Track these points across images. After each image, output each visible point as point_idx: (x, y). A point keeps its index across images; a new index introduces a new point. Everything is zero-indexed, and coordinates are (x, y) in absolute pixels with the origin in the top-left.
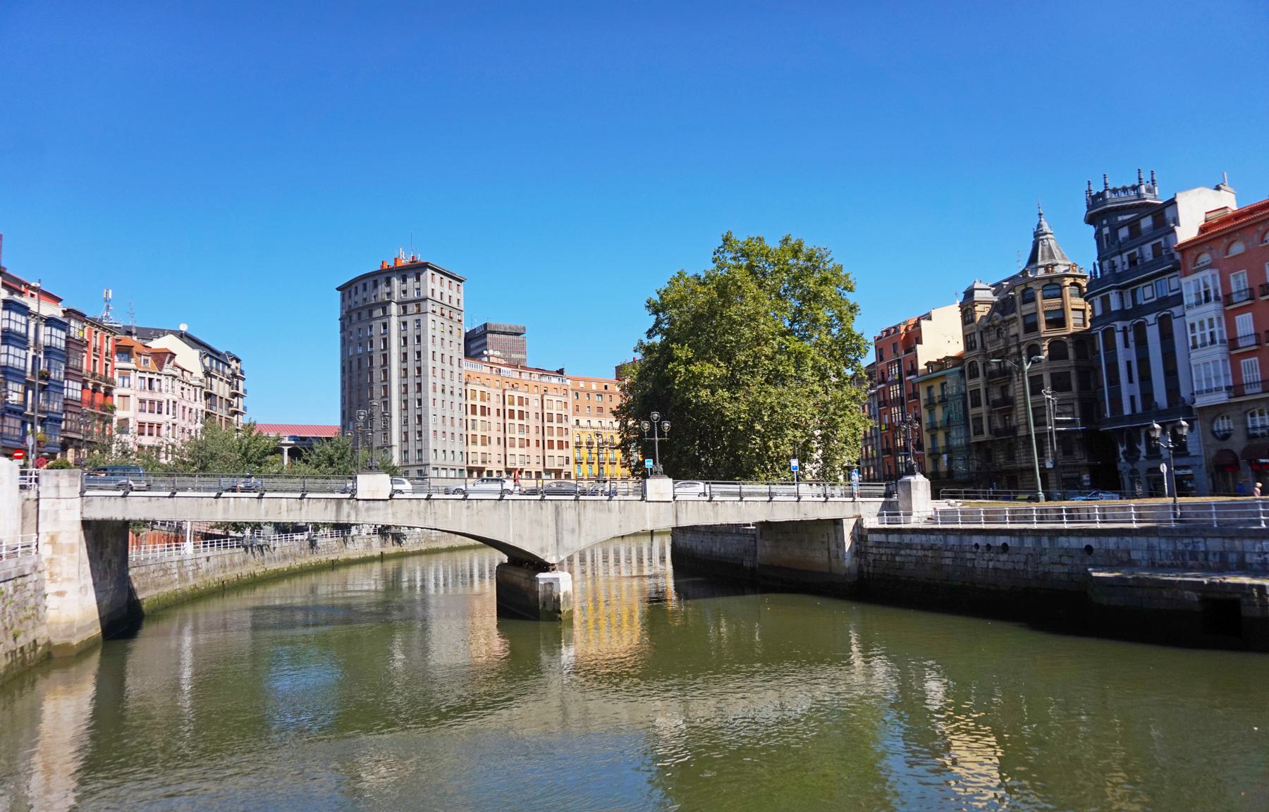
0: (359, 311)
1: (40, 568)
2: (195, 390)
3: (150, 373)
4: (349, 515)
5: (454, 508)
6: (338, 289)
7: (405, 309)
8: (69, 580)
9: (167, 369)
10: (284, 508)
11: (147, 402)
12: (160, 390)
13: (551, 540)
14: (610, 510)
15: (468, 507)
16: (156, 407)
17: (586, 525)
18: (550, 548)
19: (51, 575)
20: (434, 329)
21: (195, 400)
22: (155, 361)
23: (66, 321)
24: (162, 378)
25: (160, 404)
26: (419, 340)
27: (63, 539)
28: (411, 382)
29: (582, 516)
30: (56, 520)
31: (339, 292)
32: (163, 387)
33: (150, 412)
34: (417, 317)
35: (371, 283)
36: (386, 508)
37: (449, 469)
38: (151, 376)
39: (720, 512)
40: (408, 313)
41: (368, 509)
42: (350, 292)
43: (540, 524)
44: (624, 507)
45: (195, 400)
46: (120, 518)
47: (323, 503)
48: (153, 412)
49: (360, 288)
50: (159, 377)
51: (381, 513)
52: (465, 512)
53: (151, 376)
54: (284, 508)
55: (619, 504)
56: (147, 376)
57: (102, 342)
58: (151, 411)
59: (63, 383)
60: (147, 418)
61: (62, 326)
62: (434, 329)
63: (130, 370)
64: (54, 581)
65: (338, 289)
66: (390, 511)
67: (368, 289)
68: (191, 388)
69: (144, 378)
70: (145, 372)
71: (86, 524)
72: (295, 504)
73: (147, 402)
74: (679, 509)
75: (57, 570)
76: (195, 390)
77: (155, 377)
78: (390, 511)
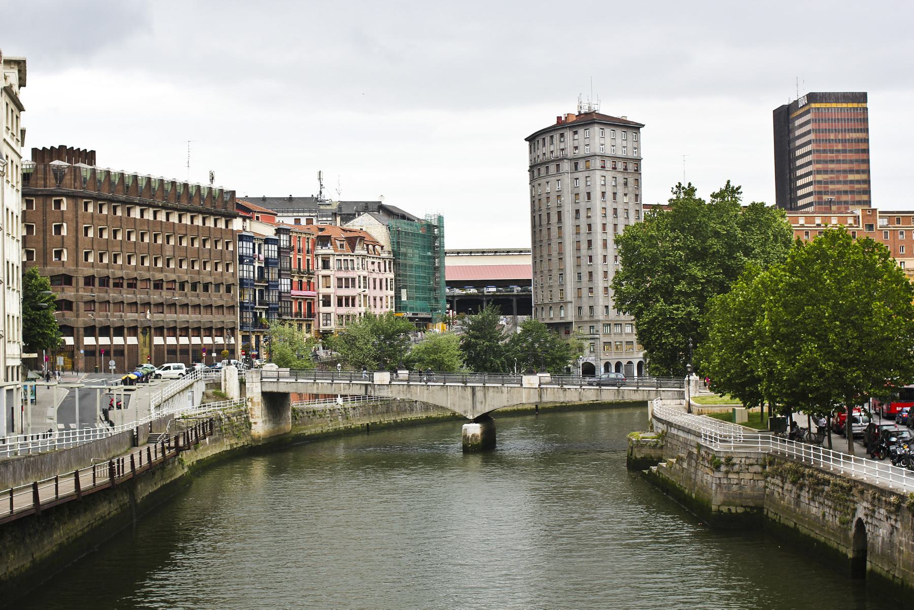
0: (546, 163)
1: (248, 412)
2: (385, 262)
3: (345, 255)
4: (371, 392)
5: (420, 389)
6: (526, 140)
7: (576, 165)
8: (258, 417)
9: (359, 250)
10: (342, 388)
11: (344, 279)
12: (353, 269)
13: (470, 407)
14: (502, 392)
15: (427, 389)
16: (349, 282)
17: (488, 399)
18: (469, 411)
19: (252, 415)
20: (604, 185)
21: (385, 271)
22: (349, 244)
23: (277, 238)
24: (354, 258)
25: (353, 280)
26: (589, 198)
27: (255, 400)
28: (584, 239)
29: (487, 395)
30: (252, 392)
31: (528, 142)
32: (356, 266)
33: (346, 287)
34: (586, 174)
35: (558, 136)
36: (388, 389)
37: (623, 323)
38: (346, 258)
39: (567, 395)
40: (579, 169)
41: (379, 389)
42: (534, 144)
43: (463, 398)
44: (510, 390)
45: (385, 271)
46: (276, 391)
47: (359, 386)
48: (342, 287)
49: (548, 139)
50: (352, 258)
51: (385, 391)
52: (426, 391)
53: (346, 258)
54: (342, 388)
55: (529, 392)
56: (343, 258)
57: (304, 244)
58: (347, 287)
59: (278, 282)
60: (344, 292)
61: (275, 242)
62: (604, 185)
63: (330, 255)
64: (253, 418)
65: (526, 140)
66: (389, 390)
67: (546, 144)
68: (381, 261)
69: (341, 260)
70: (341, 255)
71: (264, 394)
72: (347, 387)
73: (344, 279)
74: (542, 392)
75: (253, 413)
76: (385, 262)
77: (349, 258)
78: (389, 390)
